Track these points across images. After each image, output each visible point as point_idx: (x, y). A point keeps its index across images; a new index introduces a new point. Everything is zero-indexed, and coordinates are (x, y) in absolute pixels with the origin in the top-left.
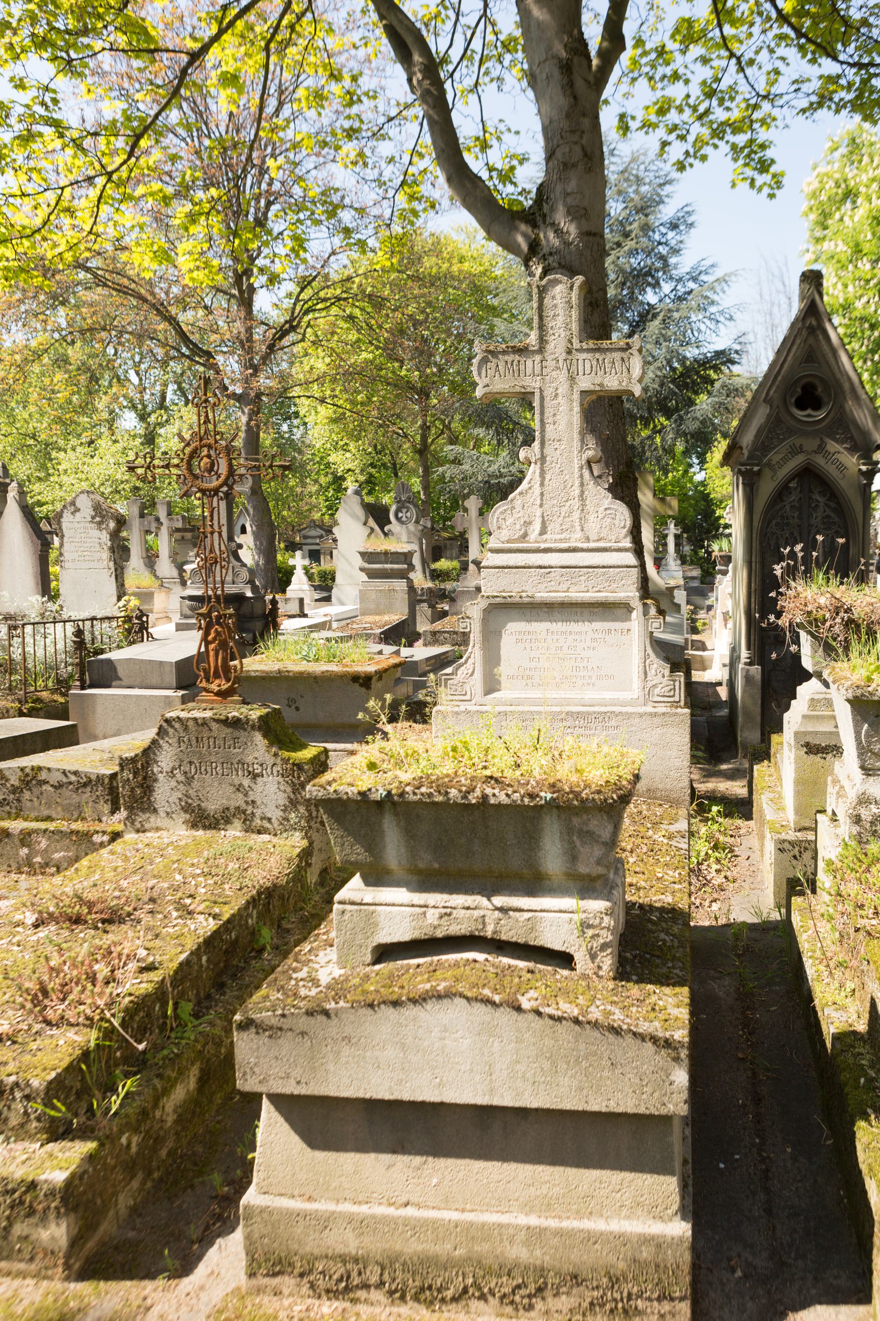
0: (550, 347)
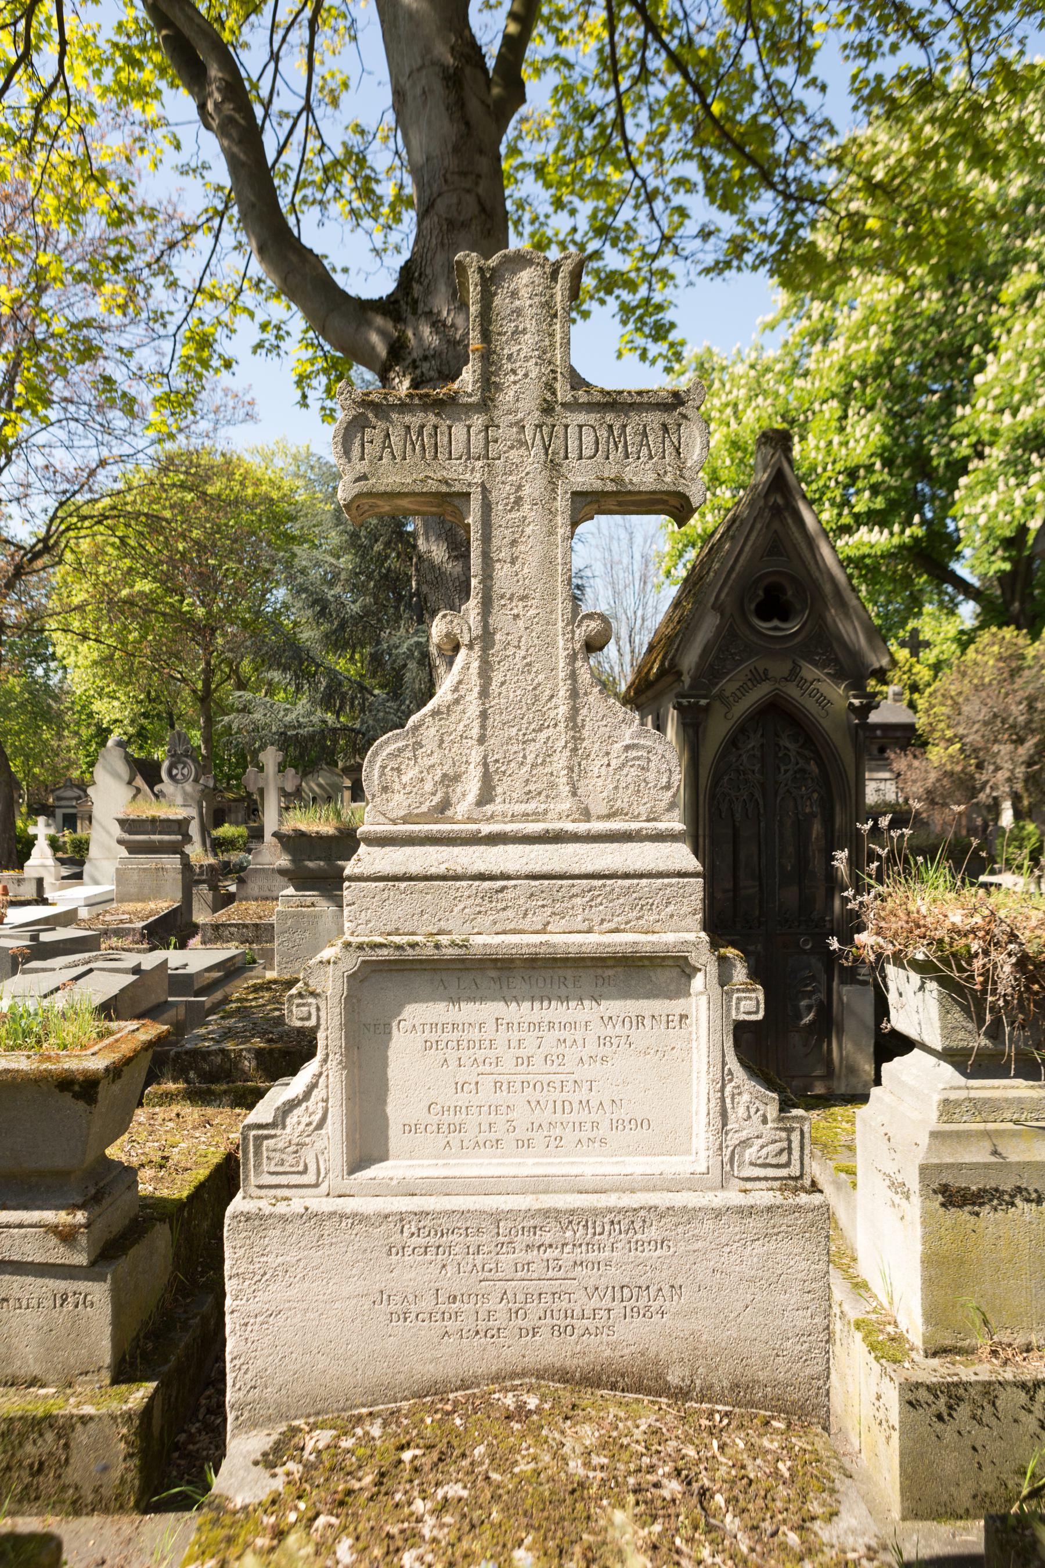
0: (506, 397)
